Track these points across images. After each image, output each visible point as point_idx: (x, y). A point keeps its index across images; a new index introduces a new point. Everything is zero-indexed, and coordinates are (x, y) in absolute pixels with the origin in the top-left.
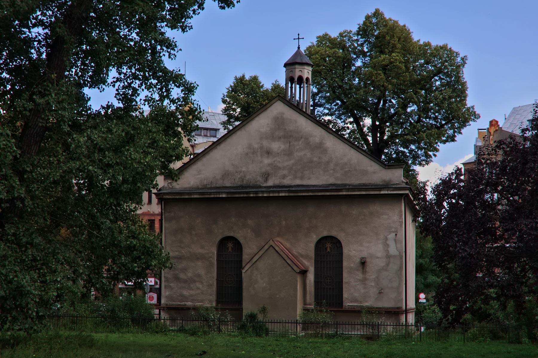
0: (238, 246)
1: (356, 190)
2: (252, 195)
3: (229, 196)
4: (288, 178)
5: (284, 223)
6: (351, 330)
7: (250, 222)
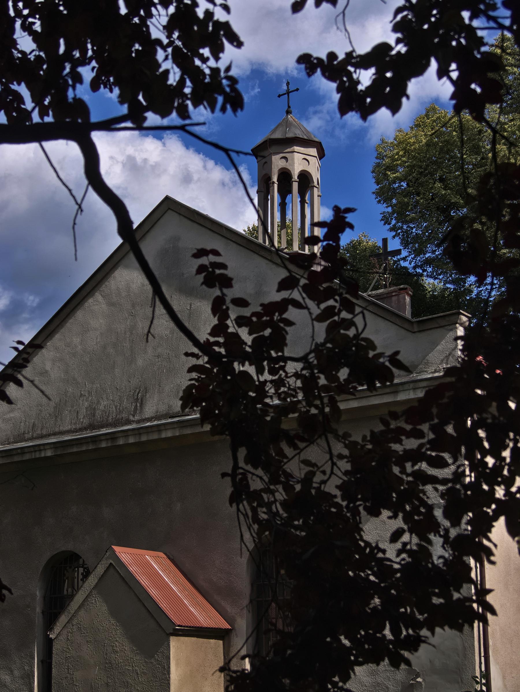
2: (104, 445)
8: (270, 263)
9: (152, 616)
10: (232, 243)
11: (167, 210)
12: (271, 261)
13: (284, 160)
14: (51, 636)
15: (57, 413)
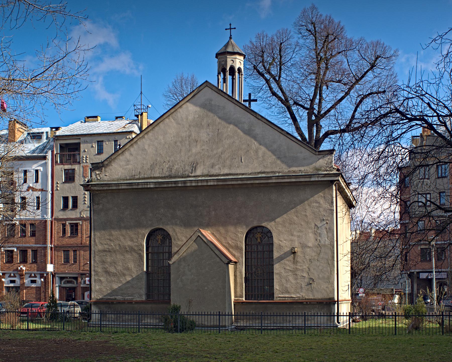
0: (167, 237)
1: (286, 177)
2: (180, 185)
3: (157, 186)
4: (217, 167)
5: (213, 213)
6: (282, 322)
7: (179, 213)
13: (232, 62)
14: (170, 263)
15: (152, 168)
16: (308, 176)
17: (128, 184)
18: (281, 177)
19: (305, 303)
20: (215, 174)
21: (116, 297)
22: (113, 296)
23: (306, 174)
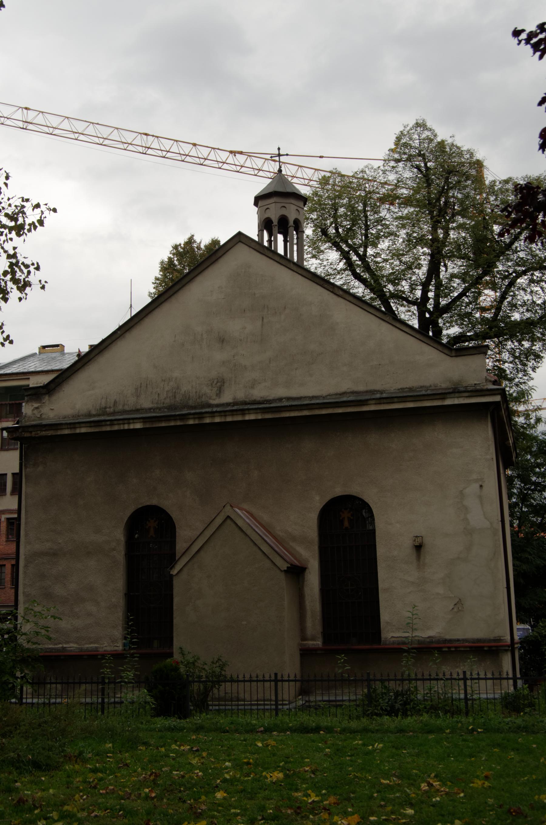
1: (396, 400)
3: (148, 426)
8: (331, 294)
9: (268, 557)
10: (297, 275)
11: (238, 243)
12: (332, 292)
16: (438, 397)
17: (92, 425)
18: (385, 401)
19: (446, 649)
20: (259, 399)
21: (65, 646)
22: (60, 643)
23: (434, 392)
